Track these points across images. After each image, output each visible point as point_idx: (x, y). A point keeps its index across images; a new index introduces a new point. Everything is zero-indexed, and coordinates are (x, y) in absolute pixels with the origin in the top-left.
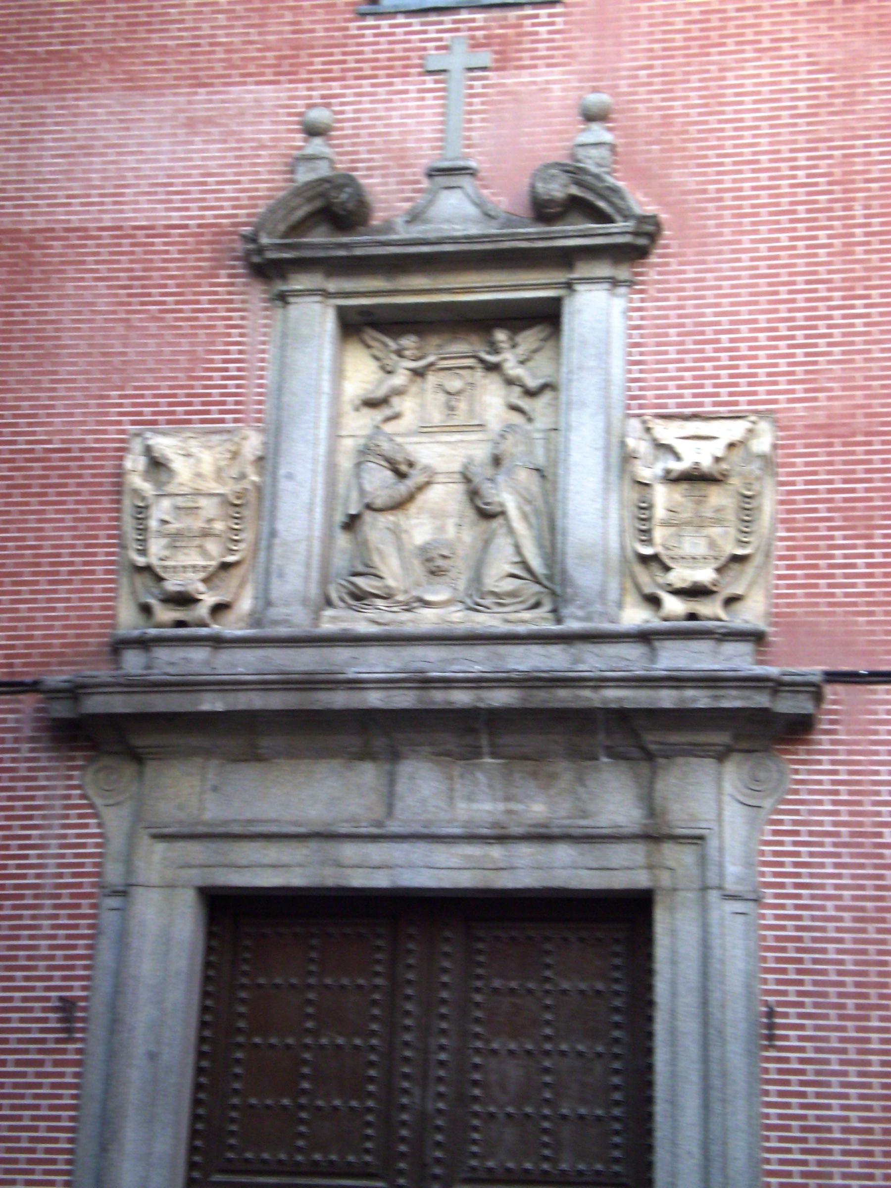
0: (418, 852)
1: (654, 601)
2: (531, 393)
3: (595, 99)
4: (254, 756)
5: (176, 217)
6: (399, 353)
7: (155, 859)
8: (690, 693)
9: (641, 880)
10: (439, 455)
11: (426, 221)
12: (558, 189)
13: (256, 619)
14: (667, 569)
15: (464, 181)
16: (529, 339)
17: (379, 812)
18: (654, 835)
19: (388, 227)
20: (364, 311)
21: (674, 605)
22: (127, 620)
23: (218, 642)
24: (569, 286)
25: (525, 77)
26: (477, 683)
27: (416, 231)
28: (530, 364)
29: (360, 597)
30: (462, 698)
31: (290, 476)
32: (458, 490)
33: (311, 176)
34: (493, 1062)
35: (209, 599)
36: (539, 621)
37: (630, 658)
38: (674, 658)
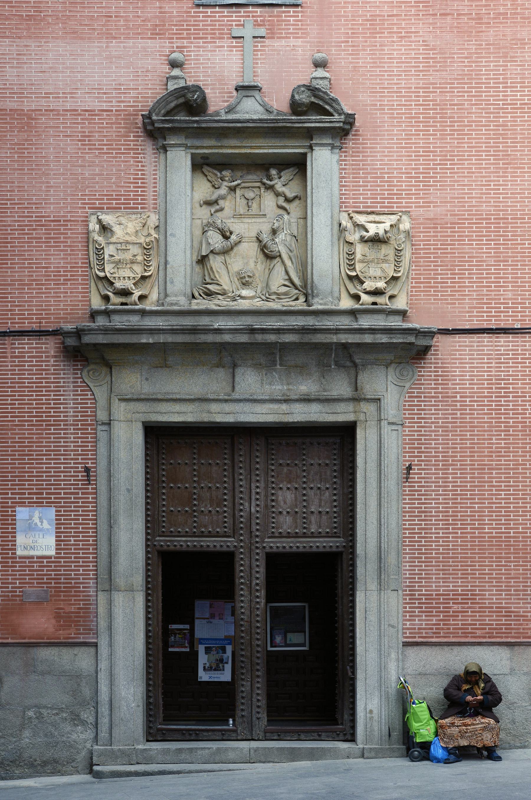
0: (247, 407)
1: (356, 298)
2: (288, 200)
3: (319, 56)
4: (165, 365)
5: (105, 106)
6: (222, 179)
7: (120, 410)
8: (379, 336)
9: (351, 418)
10: (243, 229)
11: (236, 113)
12: (304, 98)
13: (159, 302)
14: (362, 283)
15: (256, 93)
16: (287, 175)
17: (229, 389)
18: (357, 399)
19: (217, 113)
20: (205, 157)
21: (365, 298)
22: (97, 303)
23: (143, 313)
24: (311, 148)
25: (283, 42)
26: (278, 331)
27: (230, 117)
28: (288, 186)
29: (209, 294)
30: (272, 338)
31: (173, 235)
32: (255, 246)
33: (176, 86)
34: (280, 493)
35: (137, 293)
36: (300, 305)
37: (345, 322)
38: (365, 322)
